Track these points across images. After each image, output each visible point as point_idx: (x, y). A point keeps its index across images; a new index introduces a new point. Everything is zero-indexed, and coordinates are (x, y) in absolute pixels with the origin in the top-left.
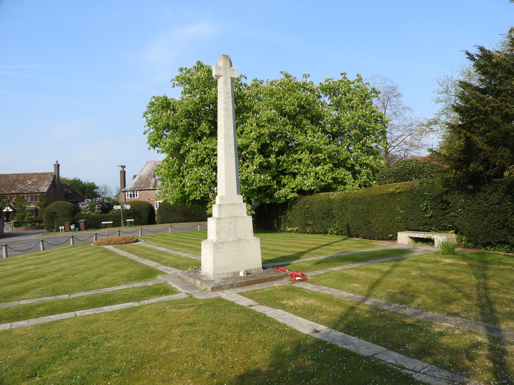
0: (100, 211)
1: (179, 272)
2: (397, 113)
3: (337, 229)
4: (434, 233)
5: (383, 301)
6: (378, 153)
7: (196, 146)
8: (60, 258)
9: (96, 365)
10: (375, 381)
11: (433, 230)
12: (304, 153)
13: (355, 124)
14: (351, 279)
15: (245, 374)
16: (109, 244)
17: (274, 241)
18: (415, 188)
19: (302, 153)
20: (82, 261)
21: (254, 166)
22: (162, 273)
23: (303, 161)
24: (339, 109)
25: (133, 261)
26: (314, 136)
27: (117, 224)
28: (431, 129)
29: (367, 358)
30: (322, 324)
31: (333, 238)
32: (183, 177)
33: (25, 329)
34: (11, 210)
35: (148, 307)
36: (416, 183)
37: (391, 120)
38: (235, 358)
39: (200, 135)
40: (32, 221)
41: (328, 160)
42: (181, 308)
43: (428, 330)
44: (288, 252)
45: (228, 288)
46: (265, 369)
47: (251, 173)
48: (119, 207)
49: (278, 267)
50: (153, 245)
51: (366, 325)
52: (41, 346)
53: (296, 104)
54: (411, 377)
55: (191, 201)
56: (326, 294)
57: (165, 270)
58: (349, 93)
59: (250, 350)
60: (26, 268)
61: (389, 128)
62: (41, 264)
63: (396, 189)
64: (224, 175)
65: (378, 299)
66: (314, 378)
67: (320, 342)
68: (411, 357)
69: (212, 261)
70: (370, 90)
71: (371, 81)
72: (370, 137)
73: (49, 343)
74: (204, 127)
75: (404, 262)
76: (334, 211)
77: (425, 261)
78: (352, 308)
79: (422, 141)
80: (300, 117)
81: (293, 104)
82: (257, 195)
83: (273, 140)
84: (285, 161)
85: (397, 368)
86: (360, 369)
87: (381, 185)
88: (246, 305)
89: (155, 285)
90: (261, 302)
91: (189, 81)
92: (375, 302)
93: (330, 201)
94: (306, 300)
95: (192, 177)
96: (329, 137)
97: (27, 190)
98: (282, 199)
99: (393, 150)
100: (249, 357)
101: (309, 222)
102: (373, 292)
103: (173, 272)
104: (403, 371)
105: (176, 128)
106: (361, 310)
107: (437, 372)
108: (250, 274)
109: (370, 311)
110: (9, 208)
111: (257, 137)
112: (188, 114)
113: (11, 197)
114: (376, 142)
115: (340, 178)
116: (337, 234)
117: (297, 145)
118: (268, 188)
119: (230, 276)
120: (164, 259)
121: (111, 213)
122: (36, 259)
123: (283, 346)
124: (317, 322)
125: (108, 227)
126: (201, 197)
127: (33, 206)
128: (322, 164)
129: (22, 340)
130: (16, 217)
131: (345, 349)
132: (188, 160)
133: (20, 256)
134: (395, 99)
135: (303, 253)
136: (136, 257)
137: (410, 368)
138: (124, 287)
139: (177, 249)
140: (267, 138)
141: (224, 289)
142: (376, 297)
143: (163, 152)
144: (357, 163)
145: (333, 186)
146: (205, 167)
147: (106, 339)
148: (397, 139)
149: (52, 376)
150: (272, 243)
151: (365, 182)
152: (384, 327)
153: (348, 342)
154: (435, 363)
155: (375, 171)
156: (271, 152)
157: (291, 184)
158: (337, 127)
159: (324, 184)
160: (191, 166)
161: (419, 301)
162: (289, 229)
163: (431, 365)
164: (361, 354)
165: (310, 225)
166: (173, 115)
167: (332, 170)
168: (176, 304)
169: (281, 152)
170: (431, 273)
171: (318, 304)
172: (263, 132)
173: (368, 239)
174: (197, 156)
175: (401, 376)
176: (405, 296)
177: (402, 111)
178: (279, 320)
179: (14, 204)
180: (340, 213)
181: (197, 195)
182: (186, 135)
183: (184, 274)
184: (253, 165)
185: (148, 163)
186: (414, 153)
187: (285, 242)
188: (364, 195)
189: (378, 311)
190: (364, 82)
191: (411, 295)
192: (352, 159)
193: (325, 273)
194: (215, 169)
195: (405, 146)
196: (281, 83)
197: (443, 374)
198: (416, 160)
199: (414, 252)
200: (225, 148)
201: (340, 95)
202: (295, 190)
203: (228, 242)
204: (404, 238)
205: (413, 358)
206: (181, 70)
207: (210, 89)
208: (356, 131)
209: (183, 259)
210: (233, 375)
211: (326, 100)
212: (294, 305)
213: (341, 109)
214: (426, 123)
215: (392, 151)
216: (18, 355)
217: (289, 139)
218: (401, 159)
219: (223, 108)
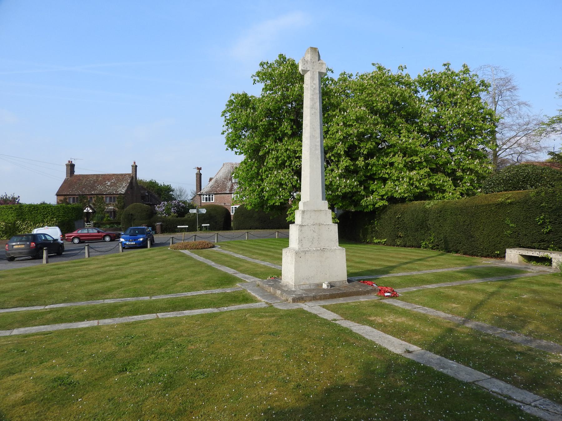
0: (176, 214)
1: (258, 281)
2: (511, 110)
3: (432, 242)
4: (552, 251)
5: (487, 325)
6: (485, 157)
7: (276, 147)
8: (139, 261)
9: (181, 365)
10: (477, 408)
11: (552, 248)
12: (397, 156)
13: (459, 123)
14: (448, 298)
15: (332, 388)
16: (185, 248)
17: (360, 253)
18: (531, 198)
19: (394, 156)
20: (160, 264)
21: (340, 169)
22: (240, 280)
23: (396, 164)
24: (440, 105)
25: (209, 267)
26: (408, 136)
27: (192, 228)
28: (554, 128)
29: (467, 384)
30: (415, 344)
31: (427, 252)
32: (262, 180)
33: (112, 326)
34: (91, 211)
35: (229, 314)
36: (531, 192)
37: (503, 118)
38: (321, 371)
39: (280, 136)
40: (110, 223)
41: (424, 164)
42: (262, 317)
43: (541, 360)
44: (376, 265)
45: (311, 300)
46: (353, 384)
47: (335, 177)
48: (194, 211)
49: (364, 281)
50: (230, 251)
51: (466, 349)
52: (128, 344)
53: (390, 100)
54: (520, 409)
55: (270, 206)
56: (420, 313)
57: (243, 277)
58: (452, 87)
59: (336, 365)
60: (108, 268)
61: (500, 127)
62: (121, 265)
63: (507, 199)
64: (308, 179)
65: (482, 322)
66: (407, 399)
67: (412, 363)
68: (520, 388)
69: (293, 270)
70: (479, 83)
71: (480, 72)
72: (476, 137)
73: (136, 341)
74: (286, 127)
75: (514, 284)
76: (429, 222)
77: (539, 283)
78: (451, 330)
79: (541, 143)
80: (393, 115)
81: (386, 101)
82: (342, 202)
83: (362, 141)
84: (374, 165)
85: (502, 397)
86: (459, 394)
87: (487, 193)
88: (330, 319)
89: (233, 292)
90: (346, 317)
91: (270, 76)
92: (477, 325)
93: (425, 211)
94: (396, 318)
95: (271, 181)
96: (426, 138)
97: (105, 191)
98: (369, 207)
99: (504, 154)
100: (336, 372)
101: (400, 233)
102: (475, 314)
103: (252, 280)
104: (509, 401)
105: (256, 128)
106: (461, 333)
107: (551, 406)
108: (333, 286)
109: (471, 335)
110: (89, 209)
111: (344, 137)
112: (269, 113)
113: (91, 198)
114: (482, 143)
115: (437, 185)
116: (432, 248)
117: (389, 147)
118: (354, 194)
119: (312, 287)
120: (241, 266)
121: (186, 217)
122: (116, 260)
123: (372, 364)
124: (410, 342)
125: (183, 231)
126: (281, 203)
127: (111, 207)
128: (417, 168)
129: (111, 336)
130: (96, 218)
131: (441, 373)
132: (267, 163)
133: (101, 257)
134: (508, 93)
135: (393, 268)
136: (213, 263)
137: (518, 399)
138: (203, 292)
139: (254, 256)
140: (355, 139)
141: (305, 301)
142: (479, 320)
143: (241, 153)
144: (459, 168)
145: (429, 194)
146: (286, 171)
147: (189, 342)
148: (508, 141)
149: (141, 372)
150: (358, 255)
151: (468, 190)
152: (488, 353)
153: (445, 366)
154: (549, 396)
155: (480, 177)
156: (359, 154)
157: (380, 190)
158: (436, 126)
159: (419, 191)
160: (271, 169)
161: (531, 327)
162: (376, 241)
163: (544, 398)
164: (460, 379)
165: (400, 237)
166: (253, 114)
167: (429, 175)
168: (257, 313)
169: (370, 155)
170: (547, 297)
171: (410, 323)
172: (351, 132)
173: (469, 255)
174: (277, 158)
175: (507, 407)
176: (515, 320)
177: (517, 107)
178: (367, 337)
179: (94, 204)
180: (437, 224)
181: (277, 201)
182: (265, 134)
183: (264, 283)
184: (338, 168)
185: (225, 166)
186: (530, 157)
187: (373, 255)
188: (467, 205)
189: (481, 335)
190: (471, 74)
191: (522, 320)
192: (453, 163)
193: (419, 291)
194: (298, 173)
195: (519, 148)
196: (372, 77)
197: (559, 409)
198: (532, 165)
199: (526, 272)
200: (311, 149)
201: (442, 89)
202: (385, 197)
203: (311, 251)
204: (513, 256)
205: (521, 389)
206: (262, 64)
207: (292, 85)
208: (459, 131)
209: (261, 268)
210: (319, 388)
211: (424, 95)
212: (383, 323)
213: (442, 105)
214: (546, 121)
215: (502, 155)
216: (109, 350)
217: (380, 140)
218: (514, 164)
219: (309, 106)
